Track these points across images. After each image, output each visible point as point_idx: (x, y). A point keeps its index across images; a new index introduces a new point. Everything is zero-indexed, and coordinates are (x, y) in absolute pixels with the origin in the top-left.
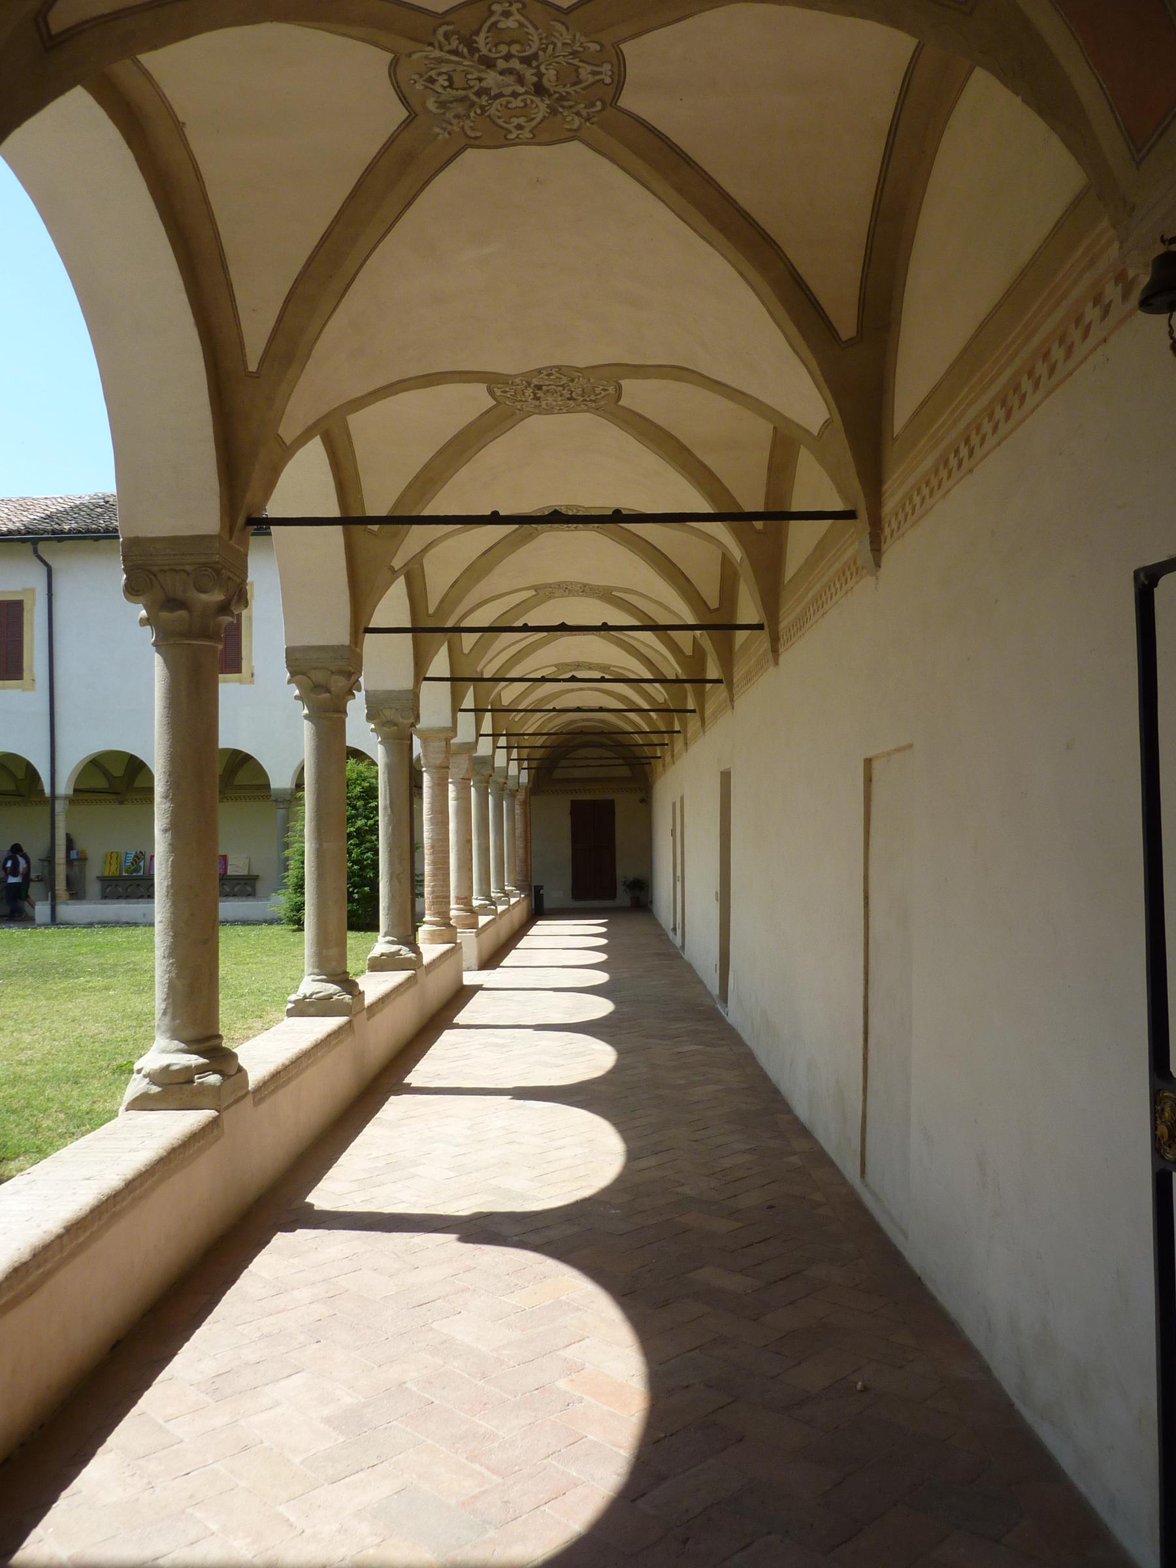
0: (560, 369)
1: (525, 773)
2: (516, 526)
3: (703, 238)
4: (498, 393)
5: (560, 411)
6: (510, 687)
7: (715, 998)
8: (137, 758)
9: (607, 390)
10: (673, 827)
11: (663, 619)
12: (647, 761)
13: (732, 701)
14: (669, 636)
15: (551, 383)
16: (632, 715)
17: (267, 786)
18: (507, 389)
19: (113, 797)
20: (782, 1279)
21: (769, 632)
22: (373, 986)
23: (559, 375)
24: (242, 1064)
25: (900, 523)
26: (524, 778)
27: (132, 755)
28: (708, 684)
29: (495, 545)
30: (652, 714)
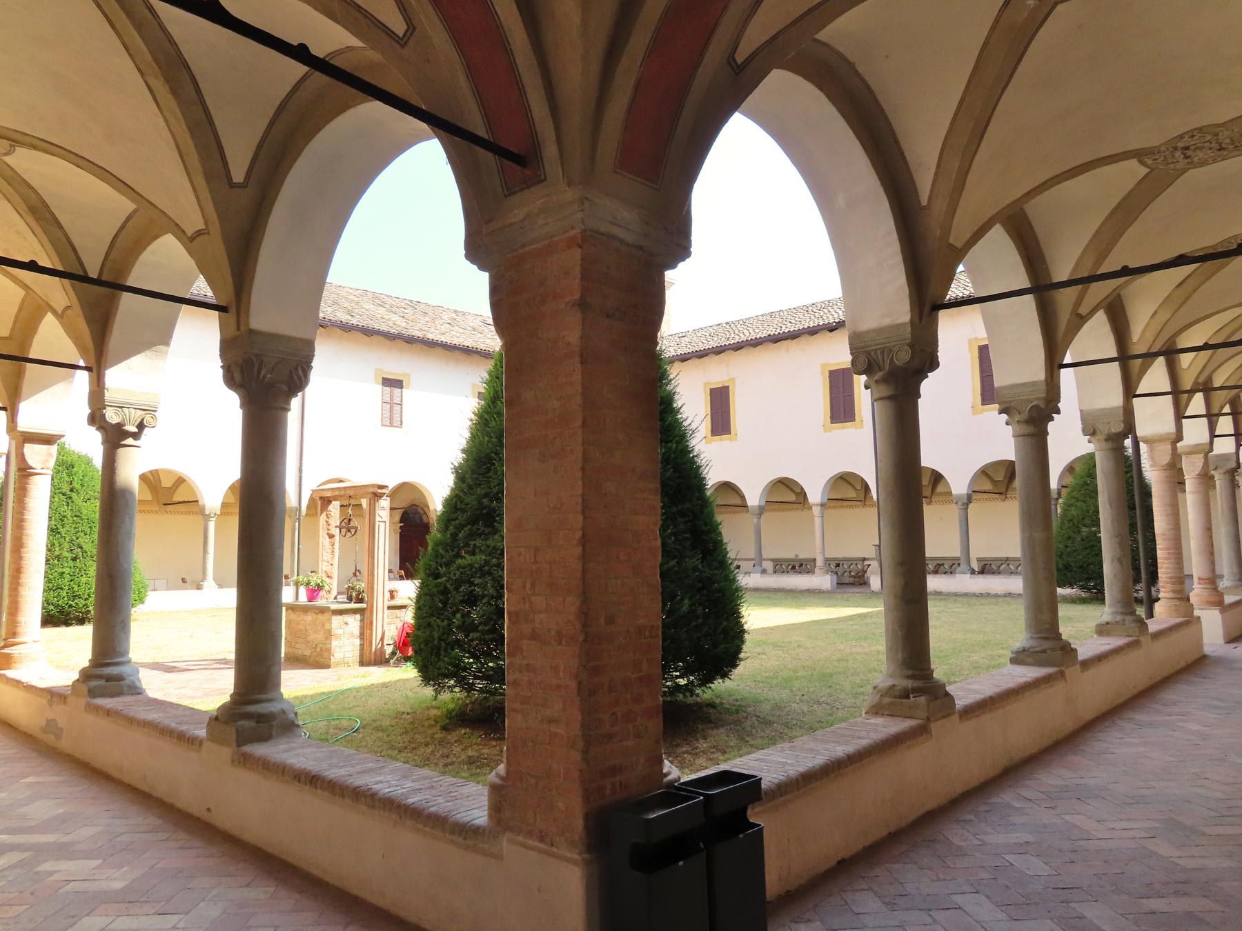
4: (1149, 162)
5: (1215, 161)
17: (950, 493)
18: (1157, 157)
19: (997, 496)
20: (881, 927)
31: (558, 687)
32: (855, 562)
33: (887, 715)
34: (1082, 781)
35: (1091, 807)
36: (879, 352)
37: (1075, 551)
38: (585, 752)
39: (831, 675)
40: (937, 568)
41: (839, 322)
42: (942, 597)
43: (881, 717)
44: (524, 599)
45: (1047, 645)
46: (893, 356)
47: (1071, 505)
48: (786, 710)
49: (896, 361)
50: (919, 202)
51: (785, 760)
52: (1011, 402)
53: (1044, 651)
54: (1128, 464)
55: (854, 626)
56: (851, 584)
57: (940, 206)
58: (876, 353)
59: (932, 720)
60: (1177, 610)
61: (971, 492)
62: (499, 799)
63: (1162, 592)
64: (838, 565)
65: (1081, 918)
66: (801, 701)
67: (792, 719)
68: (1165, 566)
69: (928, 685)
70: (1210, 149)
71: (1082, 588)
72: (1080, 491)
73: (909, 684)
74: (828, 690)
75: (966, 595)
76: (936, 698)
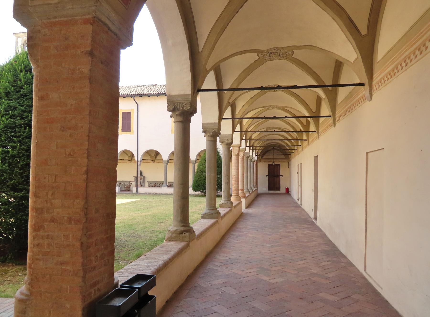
0: (277, 48)
1: (256, 157)
2: (260, 90)
3: (323, 9)
4: (260, 55)
5: (276, 59)
6: (255, 133)
7: (312, 218)
8: (158, 152)
9: (290, 53)
10: (298, 171)
11: (298, 115)
12: (290, 154)
13: (319, 137)
14: (299, 119)
15: (275, 52)
16: (286, 141)
17: (162, 160)
18: (262, 54)
20: (345, 298)
21: (333, 118)
22: (222, 211)
23: (277, 50)
24: (194, 230)
25: (379, 86)
26: (256, 158)
27: (156, 151)
28: (310, 133)
29: (255, 95)
30: (293, 141)
31: (68, 245)
32: (151, 183)
33: (174, 241)
34: (230, 257)
35: (237, 266)
36: (178, 104)
37: (201, 180)
38: (84, 277)
39: (132, 225)
40: (155, 185)
41: (128, 95)
42: (158, 195)
43: (172, 242)
44: (47, 201)
45: (213, 212)
46: (184, 106)
47: (200, 166)
48: (119, 240)
49: (184, 108)
50: (198, 49)
51: (147, 264)
52: (207, 129)
53: (212, 214)
54: (217, 153)
55: (133, 206)
56: (125, 190)
57: (205, 53)
58: (177, 104)
59: (190, 241)
60: (237, 199)
61: (169, 159)
62: (25, 307)
63: (233, 193)
64: (120, 183)
65: (254, 307)
66: (124, 236)
67: (123, 243)
68: (234, 185)
69: (189, 229)
70: (277, 55)
71: (202, 192)
72: (204, 161)
73: (183, 229)
74: (133, 231)
75: (165, 194)
76: (191, 233)
